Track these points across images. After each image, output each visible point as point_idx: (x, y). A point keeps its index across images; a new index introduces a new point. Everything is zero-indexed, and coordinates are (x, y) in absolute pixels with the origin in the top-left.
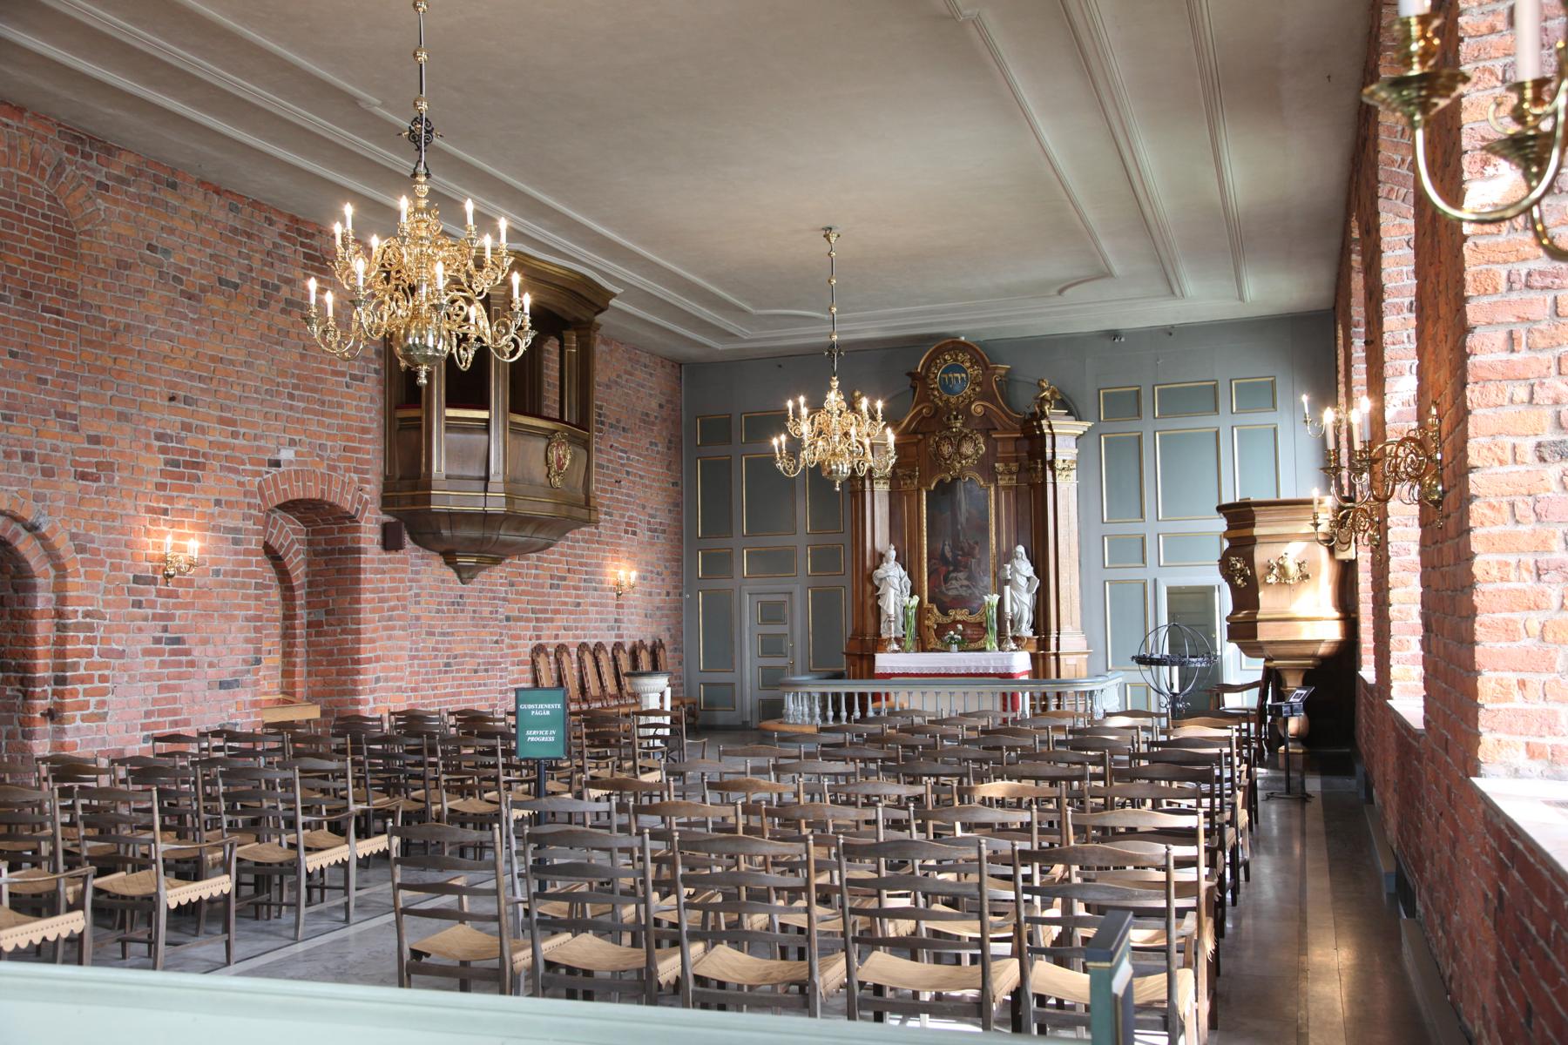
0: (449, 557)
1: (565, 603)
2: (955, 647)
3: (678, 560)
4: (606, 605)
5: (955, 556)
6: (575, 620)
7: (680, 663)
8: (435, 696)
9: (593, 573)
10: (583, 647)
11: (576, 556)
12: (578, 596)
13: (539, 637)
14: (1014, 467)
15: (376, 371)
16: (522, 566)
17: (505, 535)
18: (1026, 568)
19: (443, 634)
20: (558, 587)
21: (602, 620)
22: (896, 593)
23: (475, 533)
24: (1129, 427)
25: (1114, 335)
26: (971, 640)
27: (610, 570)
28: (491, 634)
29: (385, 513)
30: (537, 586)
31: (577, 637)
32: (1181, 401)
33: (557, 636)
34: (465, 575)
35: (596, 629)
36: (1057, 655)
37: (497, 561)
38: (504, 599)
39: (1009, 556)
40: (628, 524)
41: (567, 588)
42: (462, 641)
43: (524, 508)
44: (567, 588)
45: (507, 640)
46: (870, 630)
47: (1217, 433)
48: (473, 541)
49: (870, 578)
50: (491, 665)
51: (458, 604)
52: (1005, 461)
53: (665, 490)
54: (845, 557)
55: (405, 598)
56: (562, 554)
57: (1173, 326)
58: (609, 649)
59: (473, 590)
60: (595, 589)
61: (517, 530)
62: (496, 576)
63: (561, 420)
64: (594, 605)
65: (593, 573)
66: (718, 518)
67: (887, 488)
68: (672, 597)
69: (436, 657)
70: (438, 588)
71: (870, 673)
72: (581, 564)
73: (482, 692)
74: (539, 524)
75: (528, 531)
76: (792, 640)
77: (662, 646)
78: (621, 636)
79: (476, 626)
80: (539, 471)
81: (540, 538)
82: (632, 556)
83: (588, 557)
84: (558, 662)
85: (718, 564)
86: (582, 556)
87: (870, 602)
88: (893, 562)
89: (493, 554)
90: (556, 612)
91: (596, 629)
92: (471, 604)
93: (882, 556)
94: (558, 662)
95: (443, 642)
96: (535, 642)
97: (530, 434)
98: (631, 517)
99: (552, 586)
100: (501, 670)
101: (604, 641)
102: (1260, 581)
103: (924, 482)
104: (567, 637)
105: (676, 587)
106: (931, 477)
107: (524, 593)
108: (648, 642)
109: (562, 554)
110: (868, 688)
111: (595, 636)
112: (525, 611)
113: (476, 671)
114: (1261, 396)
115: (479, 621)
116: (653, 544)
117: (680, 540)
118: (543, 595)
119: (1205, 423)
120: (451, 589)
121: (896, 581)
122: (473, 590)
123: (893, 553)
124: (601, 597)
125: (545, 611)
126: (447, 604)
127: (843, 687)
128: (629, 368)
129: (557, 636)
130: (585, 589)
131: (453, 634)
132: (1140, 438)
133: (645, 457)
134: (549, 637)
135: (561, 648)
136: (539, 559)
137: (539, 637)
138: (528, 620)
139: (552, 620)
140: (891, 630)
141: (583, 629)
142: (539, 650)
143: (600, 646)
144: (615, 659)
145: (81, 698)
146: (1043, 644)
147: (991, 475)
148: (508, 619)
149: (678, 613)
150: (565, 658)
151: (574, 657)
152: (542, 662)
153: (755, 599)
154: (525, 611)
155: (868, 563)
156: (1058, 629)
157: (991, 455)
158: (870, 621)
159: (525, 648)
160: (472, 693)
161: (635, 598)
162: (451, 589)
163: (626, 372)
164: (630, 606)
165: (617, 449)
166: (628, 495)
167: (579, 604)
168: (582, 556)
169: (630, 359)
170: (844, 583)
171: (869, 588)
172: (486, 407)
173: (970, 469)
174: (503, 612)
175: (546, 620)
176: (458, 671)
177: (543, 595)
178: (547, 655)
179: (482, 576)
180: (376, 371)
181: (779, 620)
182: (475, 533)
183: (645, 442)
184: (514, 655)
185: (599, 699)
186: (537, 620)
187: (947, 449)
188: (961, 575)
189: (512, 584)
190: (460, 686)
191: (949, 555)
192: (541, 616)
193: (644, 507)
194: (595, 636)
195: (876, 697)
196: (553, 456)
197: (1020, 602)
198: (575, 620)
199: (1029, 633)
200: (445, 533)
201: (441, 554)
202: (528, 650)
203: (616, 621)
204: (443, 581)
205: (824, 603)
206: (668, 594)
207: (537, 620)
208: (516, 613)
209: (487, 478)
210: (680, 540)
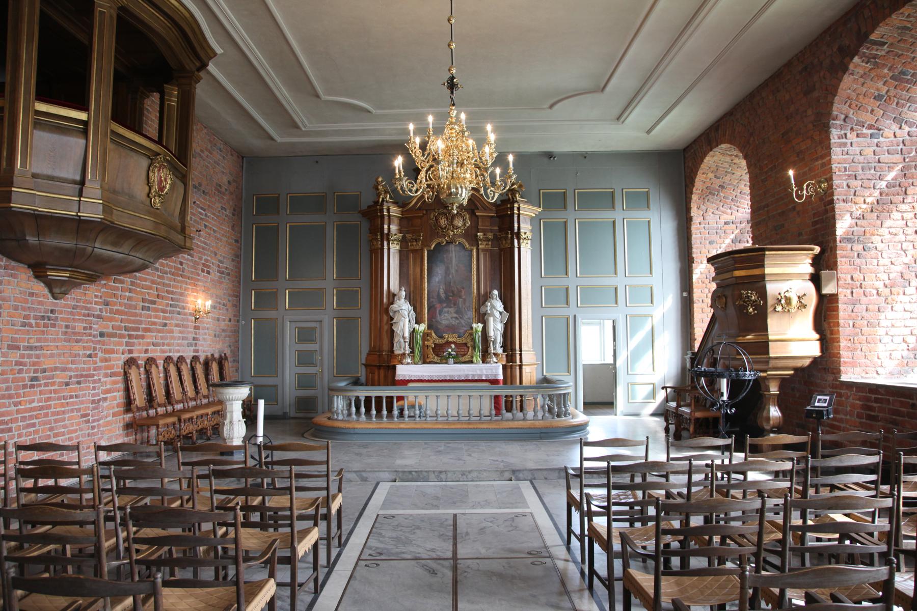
0: (39, 270)
1: (154, 323)
2: (451, 360)
3: (238, 297)
4: (186, 327)
5: (447, 297)
6: (162, 338)
7: (237, 371)
8: (18, 412)
9: (178, 300)
10: (168, 360)
11: (164, 284)
12: (165, 318)
13: (130, 352)
14: (490, 236)
16: (117, 289)
17: (101, 248)
18: (499, 306)
20: (149, 309)
21: (183, 338)
22: (405, 319)
23: (67, 243)
24: (558, 216)
25: (550, 155)
26: (462, 355)
27: (191, 299)
28: (84, 348)
30: (130, 307)
31: (163, 351)
32: (591, 201)
33: (146, 351)
34: (57, 290)
35: (179, 345)
36: (521, 366)
37: (92, 279)
38: (99, 317)
39: (487, 297)
40: (204, 265)
41: (157, 310)
42: (52, 356)
43: (123, 220)
44: (157, 310)
45: (100, 354)
46: (386, 347)
47: (614, 222)
48: (66, 251)
49: (387, 311)
50: (82, 378)
51: (49, 318)
52: (485, 232)
53: (230, 244)
54: (363, 298)
56: (153, 282)
57: (586, 153)
58: (188, 361)
59: (66, 306)
60: (179, 313)
61: (115, 244)
62: (91, 295)
63: (159, 142)
64: (177, 325)
65: (178, 300)
66: (268, 267)
67: (398, 247)
68: (232, 322)
69: (20, 371)
70: (27, 301)
71: (393, 381)
72: (168, 292)
73: (73, 404)
74: (139, 240)
75: (125, 248)
76: (321, 355)
77: (226, 358)
78: (197, 351)
79: (69, 340)
80: (140, 190)
81: (137, 257)
82: (206, 290)
83: (176, 287)
84: (148, 373)
85: (267, 300)
86: (169, 286)
87: (386, 327)
88: (403, 300)
89: (91, 270)
90: (147, 330)
91: (179, 345)
92: (63, 319)
93: (394, 295)
94: (148, 373)
95: (30, 356)
98: (206, 260)
99: (143, 308)
100: (95, 382)
101: (184, 355)
102: (770, 310)
103: (426, 243)
104: (156, 351)
105: (235, 316)
106: (431, 241)
107: (118, 312)
108: (217, 356)
109: (153, 282)
110: (393, 392)
111: (178, 351)
112: (119, 328)
113: (67, 384)
114: (641, 201)
115: (71, 335)
116: (221, 283)
117: (239, 282)
118: (135, 315)
119: (606, 215)
120: (40, 303)
121: (406, 313)
122: (66, 306)
123: (404, 293)
124: (183, 320)
125: (137, 329)
126: (35, 318)
127: (374, 392)
128: (209, 147)
129: (146, 351)
130: (171, 312)
131: (41, 348)
132: (565, 223)
133: (218, 217)
134: (140, 352)
135: (151, 361)
136: (132, 283)
137: (130, 352)
138: (121, 336)
139: (143, 337)
140: (401, 346)
141: (168, 345)
142: (130, 362)
143: (181, 359)
144: (193, 369)
146: (511, 358)
147: (474, 241)
148: (102, 335)
149: (236, 334)
150: (153, 370)
151: (161, 368)
152: (133, 373)
153: (294, 324)
154: (119, 328)
155: (385, 300)
156: (521, 351)
157: (475, 227)
158: (386, 341)
159: (118, 361)
160: (62, 405)
161: (208, 322)
162: (40, 303)
163: (207, 150)
164: (204, 328)
165: (198, 206)
166: (205, 243)
167: (165, 325)
168: (169, 286)
169: (210, 141)
170: (362, 316)
171: (385, 318)
172: (84, 108)
173: (460, 236)
175: (137, 337)
176: (46, 385)
177: (135, 315)
178: (138, 367)
179: (75, 294)
181: (312, 341)
182: (67, 243)
183: (218, 205)
184: (107, 368)
185: (182, 401)
186: (130, 336)
187: (443, 222)
188: (452, 310)
189: (107, 304)
190: (49, 399)
191: (443, 296)
192: (133, 333)
193: (216, 254)
194: (178, 351)
195: (400, 398)
196: (155, 176)
197: (496, 329)
198: (162, 338)
199: (500, 351)
200: (32, 240)
201: (30, 266)
202: (121, 363)
203: (194, 339)
204: (31, 295)
205: (345, 328)
206: (230, 320)
207: (130, 336)
208: (111, 330)
209: (82, 183)
210: (239, 282)
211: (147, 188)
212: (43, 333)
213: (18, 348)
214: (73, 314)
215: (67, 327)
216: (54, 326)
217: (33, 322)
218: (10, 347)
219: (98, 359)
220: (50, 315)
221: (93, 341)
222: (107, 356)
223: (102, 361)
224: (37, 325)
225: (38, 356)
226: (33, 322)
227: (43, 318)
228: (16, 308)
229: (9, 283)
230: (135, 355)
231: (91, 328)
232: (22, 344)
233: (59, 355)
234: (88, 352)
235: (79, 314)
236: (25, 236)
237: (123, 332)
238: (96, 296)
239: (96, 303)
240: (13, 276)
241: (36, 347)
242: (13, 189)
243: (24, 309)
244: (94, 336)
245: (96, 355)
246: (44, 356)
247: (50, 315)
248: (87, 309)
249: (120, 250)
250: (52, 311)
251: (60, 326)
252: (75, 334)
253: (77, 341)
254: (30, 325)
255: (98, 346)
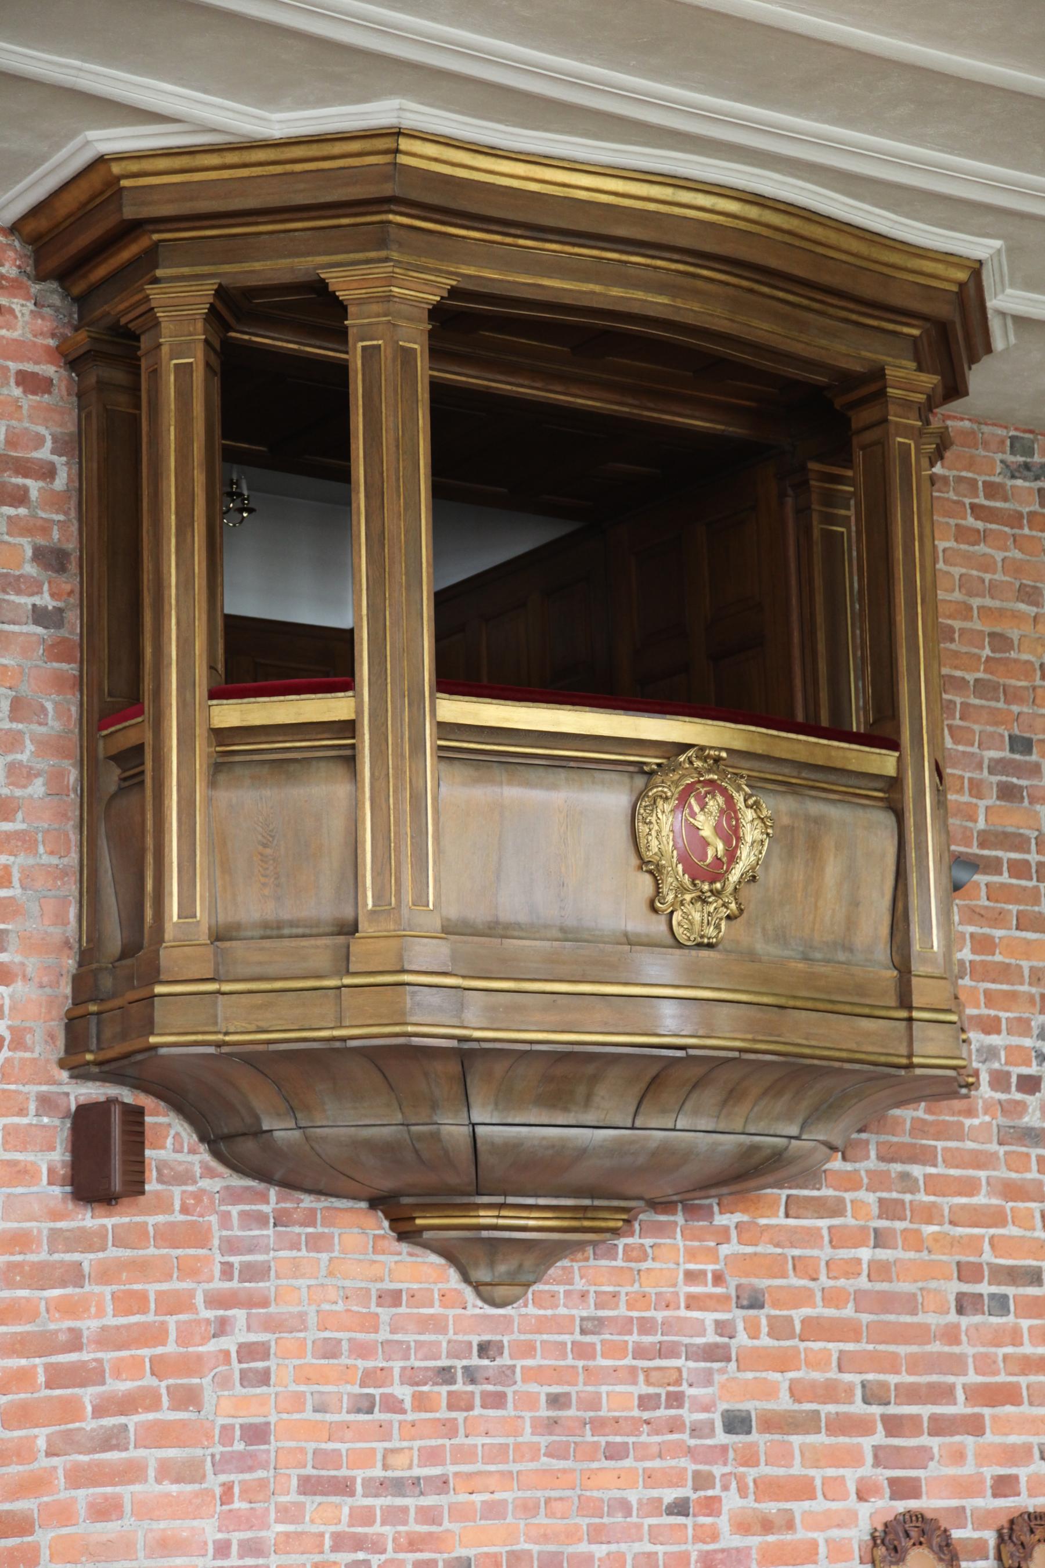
15: (40, 616)
19: (381, 1487)
28: (650, 1478)
29: (79, 1072)
30: (886, 1302)
33: (1004, 1486)
42: (493, 1510)
51: (474, 1378)
55: (192, 1365)
92: (534, 1375)
96: (888, 1507)
97: (527, 762)
122: (542, 1325)
126: (411, 1377)
131: (442, 1484)
134: (968, 1487)
136: (889, 1209)
137: (902, 1489)
145: (397, 1365)
148: (736, 1423)
162: (427, 1324)
174: (710, 1394)
177: (921, 1334)
180: (40, 616)
202: (858, 1534)
204: (394, 1298)
207: (894, 1425)
208: (784, 1402)
211: (646, 882)
212: (449, 1429)
213: (345, 1488)
214: (583, 1351)
215: (556, 1401)
216: (497, 1400)
217: (404, 1393)
218: (309, 1486)
219: (723, 1522)
220: (475, 1361)
221: (690, 1452)
222: (771, 1507)
223: (743, 1527)
224: (421, 1402)
225: (430, 1516)
226: (404, 1393)
227: (445, 1375)
228: (330, 1350)
229: (296, 1269)
230: (925, 1504)
231: (676, 1400)
232: (360, 1475)
233: (529, 1509)
234: (669, 1495)
235: (614, 1350)
236: (258, 1120)
237: (858, 1407)
238: (691, 1276)
239: (693, 1302)
240: (316, 1243)
241: (416, 1481)
242: (159, 989)
243: (362, 1350)
244: (695, 1432)
245: (711, 1506)
246: (459, 1513)
247: (475, 1361)
248: (646, 1326)
249: (590, 1118)
250: (484, 1349)
251: (529, 1401)
252: (599, 1425)
253: (615, 1453)
254: (393, 1405)
255: (718, 1470)
